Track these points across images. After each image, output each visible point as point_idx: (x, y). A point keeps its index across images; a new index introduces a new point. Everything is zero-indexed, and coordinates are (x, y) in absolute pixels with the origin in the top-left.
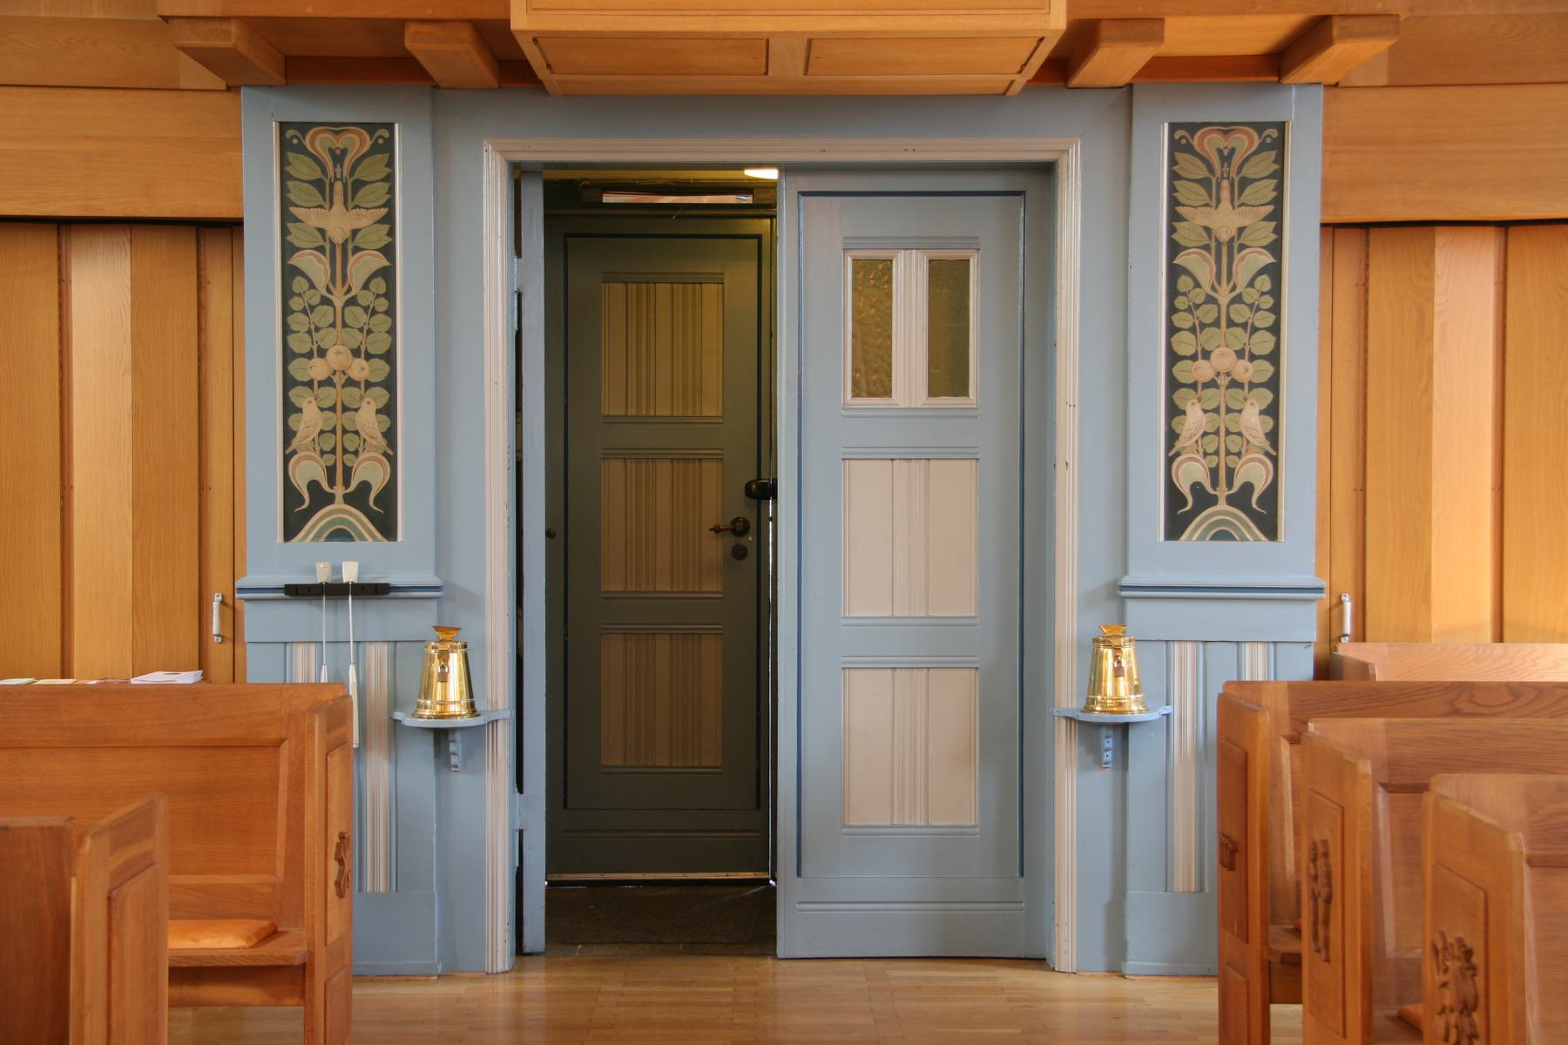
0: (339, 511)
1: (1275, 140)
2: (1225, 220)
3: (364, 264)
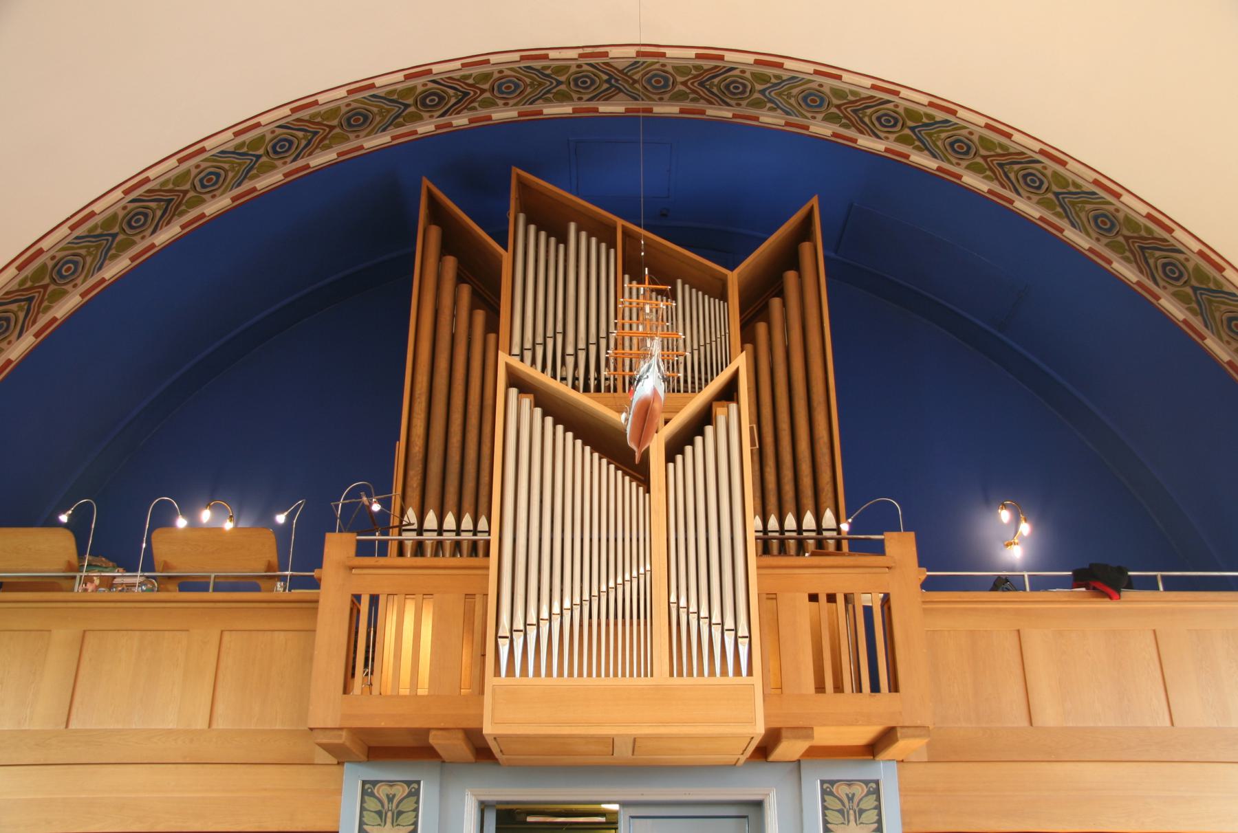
1: (875, 789)
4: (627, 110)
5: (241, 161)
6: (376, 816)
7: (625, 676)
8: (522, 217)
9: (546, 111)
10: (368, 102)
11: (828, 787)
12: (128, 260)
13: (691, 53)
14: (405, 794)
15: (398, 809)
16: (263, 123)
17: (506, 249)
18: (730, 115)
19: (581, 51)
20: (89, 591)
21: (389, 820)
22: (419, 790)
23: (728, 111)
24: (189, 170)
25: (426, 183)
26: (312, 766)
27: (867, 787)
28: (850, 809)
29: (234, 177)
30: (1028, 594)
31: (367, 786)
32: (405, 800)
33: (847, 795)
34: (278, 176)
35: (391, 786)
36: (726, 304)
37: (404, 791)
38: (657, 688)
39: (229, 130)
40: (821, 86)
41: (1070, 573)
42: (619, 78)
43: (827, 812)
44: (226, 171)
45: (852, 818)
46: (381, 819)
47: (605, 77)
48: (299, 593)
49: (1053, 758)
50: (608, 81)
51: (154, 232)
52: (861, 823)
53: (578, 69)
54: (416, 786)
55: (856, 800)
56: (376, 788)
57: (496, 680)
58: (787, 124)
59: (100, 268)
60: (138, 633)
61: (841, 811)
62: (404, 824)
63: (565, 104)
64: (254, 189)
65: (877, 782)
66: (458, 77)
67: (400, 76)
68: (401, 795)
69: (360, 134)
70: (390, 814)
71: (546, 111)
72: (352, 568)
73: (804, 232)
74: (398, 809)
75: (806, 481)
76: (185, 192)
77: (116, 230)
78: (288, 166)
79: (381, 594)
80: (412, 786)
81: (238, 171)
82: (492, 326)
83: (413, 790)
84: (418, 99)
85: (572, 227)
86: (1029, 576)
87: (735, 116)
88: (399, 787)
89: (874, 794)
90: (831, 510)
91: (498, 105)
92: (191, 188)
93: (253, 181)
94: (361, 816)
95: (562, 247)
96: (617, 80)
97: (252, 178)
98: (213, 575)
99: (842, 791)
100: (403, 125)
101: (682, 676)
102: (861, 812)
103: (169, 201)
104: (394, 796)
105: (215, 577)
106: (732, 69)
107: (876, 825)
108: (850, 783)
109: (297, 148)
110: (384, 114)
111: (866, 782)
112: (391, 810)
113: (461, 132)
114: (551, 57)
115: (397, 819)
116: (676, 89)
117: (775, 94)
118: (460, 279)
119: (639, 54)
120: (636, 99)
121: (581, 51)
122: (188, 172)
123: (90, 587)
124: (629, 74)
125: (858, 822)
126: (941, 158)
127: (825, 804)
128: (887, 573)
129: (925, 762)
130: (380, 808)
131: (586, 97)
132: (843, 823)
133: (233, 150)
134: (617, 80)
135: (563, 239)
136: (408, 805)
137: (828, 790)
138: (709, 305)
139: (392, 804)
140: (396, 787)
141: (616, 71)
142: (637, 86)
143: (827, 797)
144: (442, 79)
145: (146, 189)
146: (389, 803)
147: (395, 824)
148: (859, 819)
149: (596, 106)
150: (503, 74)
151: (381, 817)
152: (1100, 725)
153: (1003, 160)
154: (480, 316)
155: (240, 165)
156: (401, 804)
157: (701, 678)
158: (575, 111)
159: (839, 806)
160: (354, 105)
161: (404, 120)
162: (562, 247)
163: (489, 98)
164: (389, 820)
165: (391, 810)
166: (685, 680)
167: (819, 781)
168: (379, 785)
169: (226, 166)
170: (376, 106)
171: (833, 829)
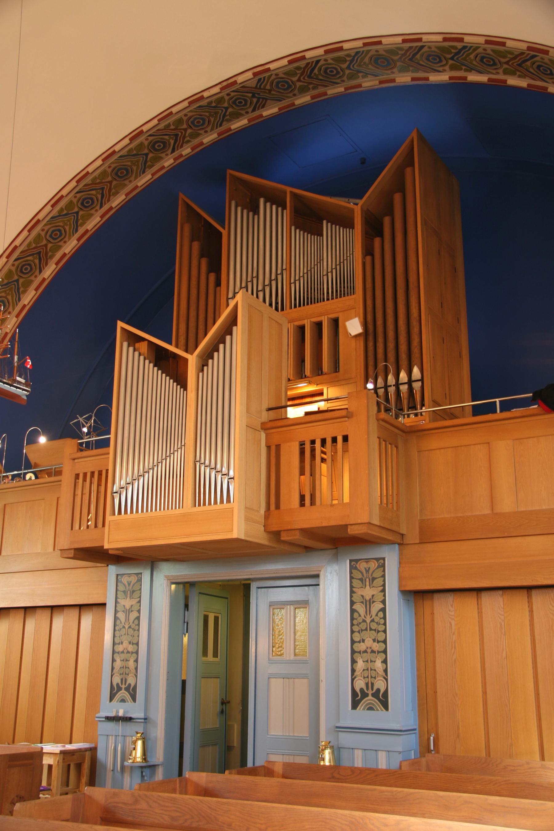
0: (123, 693)
2: (368, 592)
3: (134, 615)
4: (280, 109)
5: (68, 218)
6: (123, 594)
7: (173, 509)
8: (233, 203)
9: (233, 127)
10: (121, 161)
11: (354, 564)
12: (34, 291)
13: (285, 62)
14: (376, 567)
15: (372, 576)
16: (64, 195)
17: (224, 228)
18: (342, 89)
19: (220, 86)
20: (6, 483)
21: (129, 596)
22: (384, 564)
23: (341, 87)
24: (39, 233)
25: (182, 196)
26: (97, 568)
27: (378, 563)
28: (367, 578)
29: (70, 229)
30: (499, 414)
31: (352, 563)
32: (374, 573)
33: (365, 569)
34: (97, 219)
35: (129, 576)
36: (321, 238)
37: (375, 565)
38: (184, 515)
39: (48, 205)
40: (377, 51)
41: (531, 394)
42: (259, 92)
43: (353, 580)
44: (63, 227)
45: (368, 583)
46: (363, 584)
47: (250, 95)
48: (53, 479)
49: (506, 535)
50: (254, 96)
51: (40, 272)
52: (373, 587)
53: (229, 97)
54: (382, 561)
55: (371, 571)
56: (358, 564)
57: (113, 518)
58: (381, 82)
59: (19, 300)
60: (25, 503)
61: (361, 580)
62: (135, 598)
63: (241, 119)
64: (87, 231)
65: (384, 559)
66: (163, 128)
67: (127, 141)
68: (134, 582)
69: (131, 179)
70: (129, 592)
71: (233, 127)
72: (74, 459)
73: (409, 161)
74: (372, 576)
75: (403, 348)
76: (46, 246)
77: (16, 277)
78: (99, 212)
79: (88, 472)
80: (380, 561)
81: (70, 224)
82: (218, 283)
83: (380, 564)
84: (150, 148)
85: (262, 201)
86: (500, 401)
87: (346, 89)
88: (372, 563)
89: (382, 567)
90: (418, 367)
91: (201, 134)
92: (47, 242)
93: (85, 226)
94: (351, 582)
95: (256, 217)
96: (259, 94)
97: (82, 225)
98: (54, 467)
99: (362, 566)
100: (153, 166)
101: (200, 506)
102: (374, 579)
103: (39, 253)
104: (131, 582)
105: (55, 468)
106: (318, 62)
107: (382, 588)
108: (367, 560)
109: (97, 200)
110: (136, 164)
111: (377, 559)
112: (368, 578)
113: (190, 159)
114: (345, 48)
115: (372, 583)
116: (298, 86)
117: (357, 66)
118: (202, 255)
119: (255, 74)
120: (281, 101)
121: (220, 86)
122: (39, 235)
123: (6, 481)
124: (262, 87)
125: (371, 586)
126: (485, 72)
127: (352, 575)
128: (346, 421)
129: (418, 543)
130: (124, 589)
131: (250, 110)
132: (362, 587)
133: (58, 215)
134: (259, 94)
135: (256, 211)
136: (378, 573)
137: (354, 566)
138: (342, 232)
139: (130, 587)
140: (132, 577)
141: (253, 89)
142: (273, 92)
143: (353, 571)
144: (154, 132)
145: (20, 251)
146: (128, 586)
147: (131, 598)
148: (372, 585)
149: (260, 113)
150: (188, 116)
151: (125, 594)
152: (544, 508)
153: (106, 191)
154: (212, 276)
155: (68, 221)
156: (134, 587)
157: (228, 504)
158: (249, 121)
159: (360, 576)
160: (113, 166)
161: (151, 162)
162: (256, 217)
163: (192, 132)
164: (129, 596)
165: (129, 590)
166: (202, 508)
167: (348, 561)
168: (360, 561)
169: (61, 224)
170: (128, 161)
171: (120, 602)
